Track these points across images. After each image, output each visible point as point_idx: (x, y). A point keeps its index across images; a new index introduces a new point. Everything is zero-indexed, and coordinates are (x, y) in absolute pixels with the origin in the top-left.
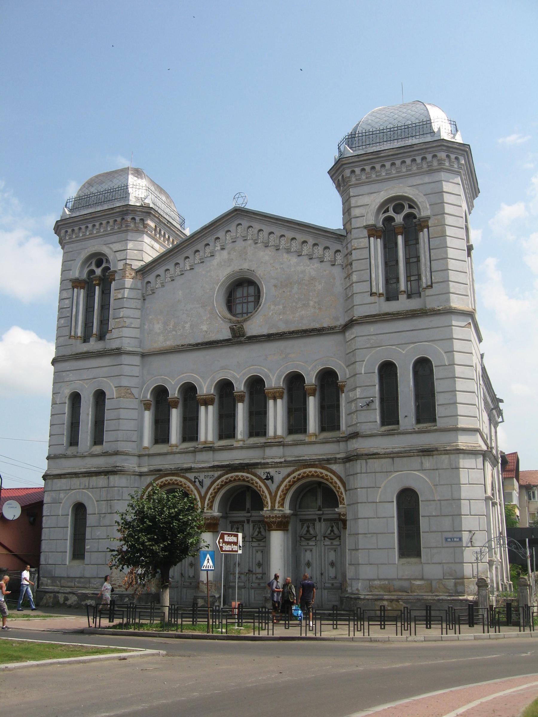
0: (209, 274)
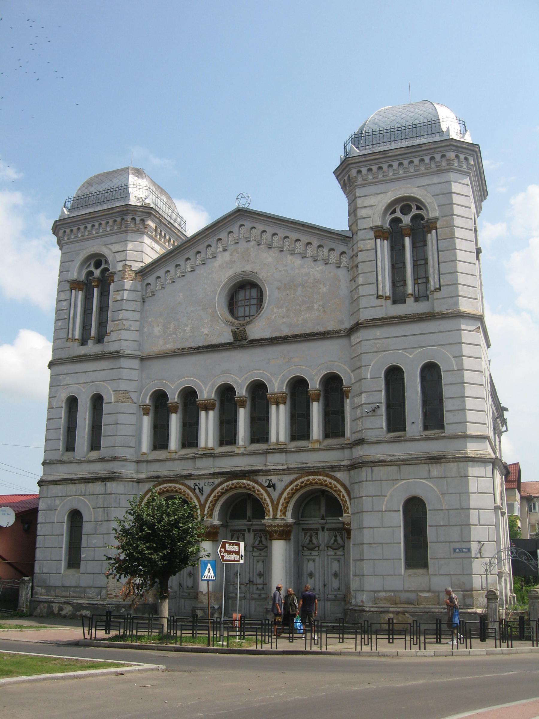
0: (210, 276)
